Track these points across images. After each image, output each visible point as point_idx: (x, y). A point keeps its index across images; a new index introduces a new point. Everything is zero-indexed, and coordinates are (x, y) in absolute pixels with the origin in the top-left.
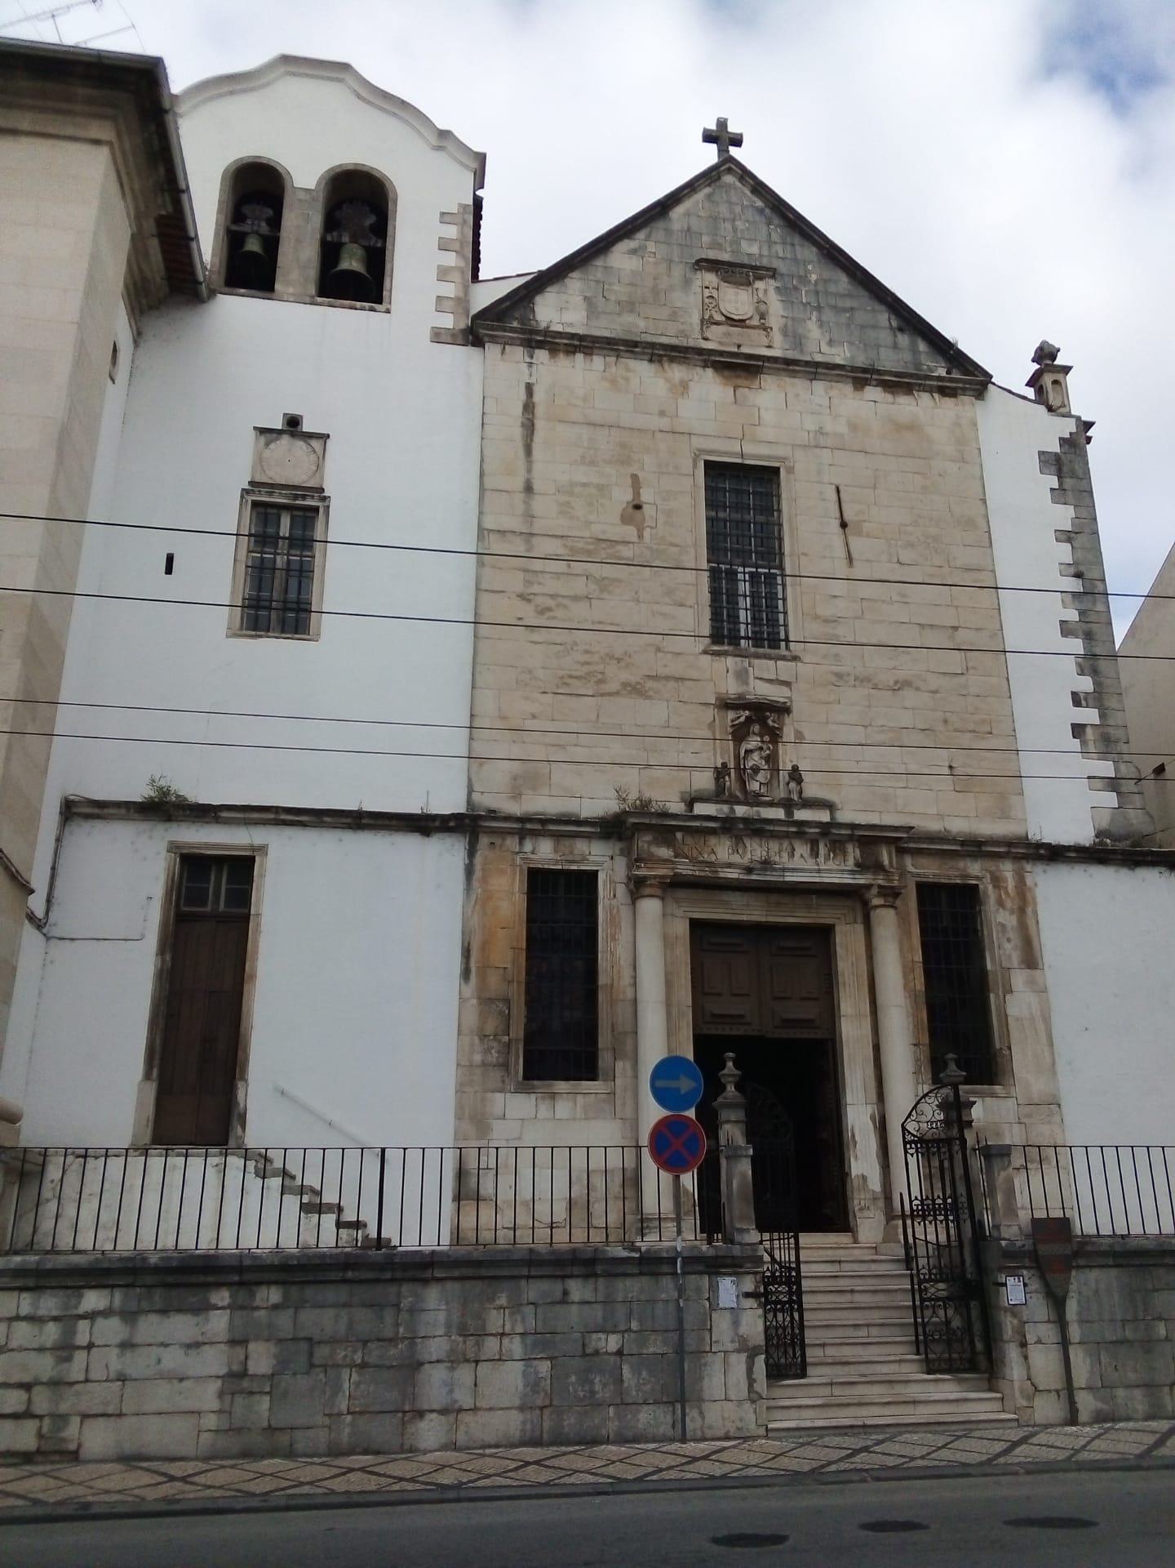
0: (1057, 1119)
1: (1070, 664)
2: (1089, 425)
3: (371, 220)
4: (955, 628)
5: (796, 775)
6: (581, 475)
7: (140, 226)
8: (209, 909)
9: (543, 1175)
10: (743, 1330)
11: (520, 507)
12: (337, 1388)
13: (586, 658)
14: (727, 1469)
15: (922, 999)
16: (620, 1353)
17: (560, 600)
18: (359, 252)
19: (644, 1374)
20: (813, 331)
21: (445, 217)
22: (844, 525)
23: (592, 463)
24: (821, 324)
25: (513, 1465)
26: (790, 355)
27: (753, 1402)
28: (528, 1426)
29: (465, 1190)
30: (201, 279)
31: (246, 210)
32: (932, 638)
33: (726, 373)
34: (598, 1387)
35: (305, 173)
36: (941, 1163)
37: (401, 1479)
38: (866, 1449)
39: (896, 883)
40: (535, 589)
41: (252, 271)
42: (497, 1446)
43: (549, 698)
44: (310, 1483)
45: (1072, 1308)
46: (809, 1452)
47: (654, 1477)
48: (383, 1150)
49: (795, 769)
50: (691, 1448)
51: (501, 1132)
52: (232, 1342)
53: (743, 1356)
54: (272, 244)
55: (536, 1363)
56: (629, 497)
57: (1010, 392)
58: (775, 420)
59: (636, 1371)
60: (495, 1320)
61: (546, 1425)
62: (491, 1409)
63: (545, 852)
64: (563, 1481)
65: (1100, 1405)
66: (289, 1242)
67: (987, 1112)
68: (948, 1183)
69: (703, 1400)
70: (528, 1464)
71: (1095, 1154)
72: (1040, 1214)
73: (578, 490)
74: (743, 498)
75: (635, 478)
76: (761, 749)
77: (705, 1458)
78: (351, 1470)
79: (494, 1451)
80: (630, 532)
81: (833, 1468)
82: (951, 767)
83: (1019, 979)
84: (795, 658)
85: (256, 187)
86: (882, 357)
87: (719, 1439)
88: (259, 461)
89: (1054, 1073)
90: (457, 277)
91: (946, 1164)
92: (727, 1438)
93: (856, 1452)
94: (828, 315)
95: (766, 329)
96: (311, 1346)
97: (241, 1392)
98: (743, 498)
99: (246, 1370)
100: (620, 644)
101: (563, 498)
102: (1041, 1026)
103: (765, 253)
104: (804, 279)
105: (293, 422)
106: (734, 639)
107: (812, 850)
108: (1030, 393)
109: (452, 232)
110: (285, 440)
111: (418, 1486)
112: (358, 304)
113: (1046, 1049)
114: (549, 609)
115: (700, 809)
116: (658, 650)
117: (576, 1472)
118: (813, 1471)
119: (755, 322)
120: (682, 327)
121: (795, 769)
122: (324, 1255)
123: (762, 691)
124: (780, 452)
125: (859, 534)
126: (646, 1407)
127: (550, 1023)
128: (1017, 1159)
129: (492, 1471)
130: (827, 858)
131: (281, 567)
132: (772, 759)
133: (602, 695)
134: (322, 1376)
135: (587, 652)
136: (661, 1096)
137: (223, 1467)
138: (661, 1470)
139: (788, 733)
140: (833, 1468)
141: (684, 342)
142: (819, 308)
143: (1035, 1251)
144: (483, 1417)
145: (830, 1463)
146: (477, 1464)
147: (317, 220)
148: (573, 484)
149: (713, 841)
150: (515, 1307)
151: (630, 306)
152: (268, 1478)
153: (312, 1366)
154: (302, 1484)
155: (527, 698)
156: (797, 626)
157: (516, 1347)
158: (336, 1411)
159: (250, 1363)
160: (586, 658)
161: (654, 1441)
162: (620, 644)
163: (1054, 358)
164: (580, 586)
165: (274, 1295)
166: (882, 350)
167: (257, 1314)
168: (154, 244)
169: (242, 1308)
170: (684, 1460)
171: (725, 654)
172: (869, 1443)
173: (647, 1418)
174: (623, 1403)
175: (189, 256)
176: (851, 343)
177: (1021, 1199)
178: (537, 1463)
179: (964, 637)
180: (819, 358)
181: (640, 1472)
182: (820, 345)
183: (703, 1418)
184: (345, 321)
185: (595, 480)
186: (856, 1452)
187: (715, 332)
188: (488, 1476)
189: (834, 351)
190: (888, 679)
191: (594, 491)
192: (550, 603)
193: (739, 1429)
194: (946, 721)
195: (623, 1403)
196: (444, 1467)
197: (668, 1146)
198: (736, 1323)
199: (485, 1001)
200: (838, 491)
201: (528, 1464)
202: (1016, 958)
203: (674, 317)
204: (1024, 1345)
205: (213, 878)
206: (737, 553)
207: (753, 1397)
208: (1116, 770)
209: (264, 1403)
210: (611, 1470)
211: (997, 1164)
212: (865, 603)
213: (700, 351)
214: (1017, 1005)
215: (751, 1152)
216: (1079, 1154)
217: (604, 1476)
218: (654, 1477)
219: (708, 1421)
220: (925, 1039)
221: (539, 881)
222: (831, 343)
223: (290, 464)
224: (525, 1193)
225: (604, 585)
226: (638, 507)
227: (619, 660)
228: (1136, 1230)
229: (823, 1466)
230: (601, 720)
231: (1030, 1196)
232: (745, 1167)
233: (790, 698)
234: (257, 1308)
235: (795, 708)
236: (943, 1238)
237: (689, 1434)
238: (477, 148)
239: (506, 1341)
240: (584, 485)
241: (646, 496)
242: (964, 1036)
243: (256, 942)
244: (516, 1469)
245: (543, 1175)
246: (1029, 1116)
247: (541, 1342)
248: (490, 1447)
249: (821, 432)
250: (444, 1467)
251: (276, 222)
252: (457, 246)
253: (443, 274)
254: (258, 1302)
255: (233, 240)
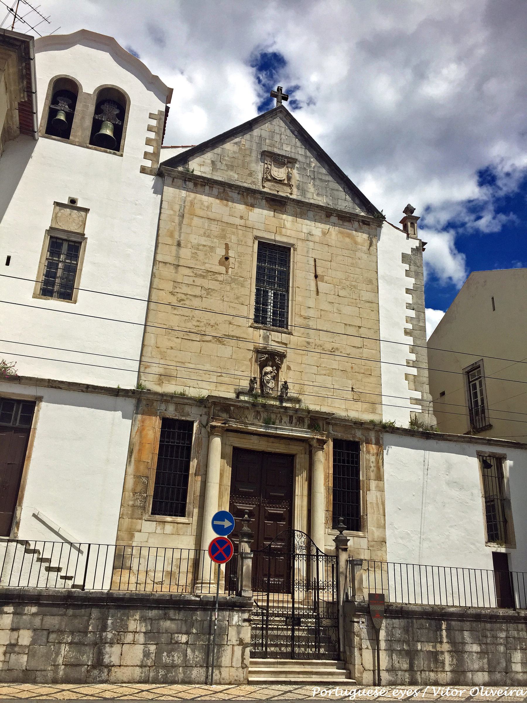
0: (384, 549)
1: (407, 349)
2: (424, 244)
3: (117, 112)
4: (360, 327)
5: (285, 386)
6: (203, 241)
7: (11, 105)
8: (11, 424)
9: (160, 559)
10: (241, 636)
11: (174, 253)
12: (58, 654)
13: (198, 324)
14: (230, 697)
15: (331, 491)
16: (187, 643)
17: (188, 296)
18: (110, 124)
19: (197, 653)
20: (311, 188)
21: (151, 116)
22: (316, 277)
23: (208, 236)
24: (314, 185)
25: (137, 691)
26: (299, 198)
27: (243, 668)
28: (143, 675)
29: (121, 562)
30: (36, 130)
31: (59, 99)
32: (351, 331)
33: (271, 203)
34: (176, 658)
35: (89, 87)
36: (333, 565)
37: (87, 695)
38: (290, 691)
39: (325, 438)
40: (177, 290)
41: (59, 129)
42: (129, 683)
43: (179, 340)
44: (47, 695)
45: (382, 634)
46: (266, 692)
47: (199, 699)
48: (90, 545)
49: (286, 383)
50: (215, 687)
51: (138, 539)
52: (13, 630)
53: (241, 648)
54: (70, 117)
55: (149, 646)
56: (223, 253)
57: (392, 225)
58: (289, 228)
59: (193, 651)
60: (132, 625)
61: (151, 674)
62: (127, 666)
63: (171, 412)
64: (159, 698)
65: (391, 678)
66: (42, 585)
67: (356, 542)
68: (335, 575)
69: (220, 666)
70: (143, 691)
71: (397, 567)
72: (373, 592)
73: (201, 247)
74: (274, 259)
75: (227, 245)
76: (272, 372)
77: (221, 692)
78: (64, 690)
79: (127, 685)
80: (223, 269)
81: (276, 698)
82: (352, 388)
83: (373, 484)
84: (290, 334)
85: (65, 90)
86: (339, 204)
87: (226, 684)
88: (55, 218)
89: (385, 528)
90: (155, 144)
91: (335, 566)
92: (230, 684)
93: (286, 692)
94: (318, 182)
95: (290, 186)
96: (49, 633)
97: (14, 652)
98: (274, 259)
99: (18, 642)
100: (213, 319)
101: (194, 251)
102: (381, 507)
103: (293, 151)
104: (309, 165)
105: (73, 201)
106: (264, 323)
107: (290, 420)
108: (401, 227)
109: (154, 123)
110: (68, 211)
111: (95, 698)
112: (108, 150)
113: (382, 517)
114: (183, 300)
115: (242, 398)
116: (230, 323)
117: (164, 695)
118: (267, 699)
119: (286, 182)
120: (254, 180)
121: (286, 383)
122: (58, 591)
123: (273, 346)
124: (291, 241)
125: (322, 281)
126: (196, 668)
127: (167, 489)
128: (365, 565)
129: (127, 693)
130: (296, 424)
131: (61, 267)
132: (276, 378)
133: (203, 341)
134: (52, 647)
135: (198, 321)
136: (217, 529)
137: (4, 687)
138: (202, 696)
139: (284, 366)
140: (276, 698)
141: (253, 187)
142: (314, 179)
143: (369, 607)
144: (124, 670)
145: (274, 697)
146: (121, 690)
147: (92, 108)
148: (199, 245)
149: (246, 412)
150: (143, 619)
151: (231, 167)
152: (25, 692)
153: (48, 642)
154: (42, 695)
155: (169, 340)
156: (293, 319)
157: (141, 638)
158: (57, 663)
159: (20, 640)
160: (198, 324)
161: (198, 683)
162: (213, 319)
163: (412, 212)
164: (197, 291)
165: (34, 609)
166: (340, 201)
167: (24, 617)
168: (16, 112)
169: (18, 614)
170: (212, 692)
171: (259, 328)
172: (292, 689)
173: (197, 673)
174: (187, 666)
175: (32, 120)
176: (327, 196)
177: (365, 584)
178: (147, 691)
179: (363, 332)
180: (312, 201)
181: (193, 696)
182: (314, 196)
183: (221, 674)
184: (101, 157)
185: (209, 244)
186: (286, 692)
187: (268, 184)
188: (126, 695)
189: (319, 198)
190: (328, 346)
191: (208, 249)
192: (183, 297)
193: (236, 680)
194: (352, 368)
195: (187, 666)
196: (106, 690)
197: (218, 551)
198: (239, 633)
199: (137, 477)
200: (315, 261)
201: (143, 691)
202: (372, 475)
203: (250, 175)
204: (360, 649)
205: (15, 409)
206: (269, 283)
207: (244, 666)
208: (422, 396)
209: (25, 657)
210: (180, 695)
211: (357, 568)
212: (323, 312)
213: (261, 193)
214: (370, 497)
215: (252, 556)
216: (391, 566)
217: (177, 697)
218: (199, 699)
219: (223, 676)
220: (331, 509)
221: (167, 423)
222: (318, 194)
223: (69, 223)
224: (151, 566)
225: (209, 291)
226: (227, 259)
227: (212, 326)
228: (412, 601)
229: (271, 698)
230: (202, 353)
231: (368, 583)
232: (249, 563)
233: (286, 351)
234: (25, 614)
235: (288, 355)
236: (330, 599)
237: (214, 681)
238: (169, 85)
239: (137, 635)
240: (204, 246)
241: (231, 254)
242: (348, 512)
243: (33, 441)
244: (138, 693)
245: (160, 559)
246: (373, 546)
247: (151, 635)
248: (125, 683)
249: (310, 234)
250: (106, 690)
251: (73, 106)
252: (156, 130)
253: (148, 142)
254: (26, 612)
255: (52, 113)
